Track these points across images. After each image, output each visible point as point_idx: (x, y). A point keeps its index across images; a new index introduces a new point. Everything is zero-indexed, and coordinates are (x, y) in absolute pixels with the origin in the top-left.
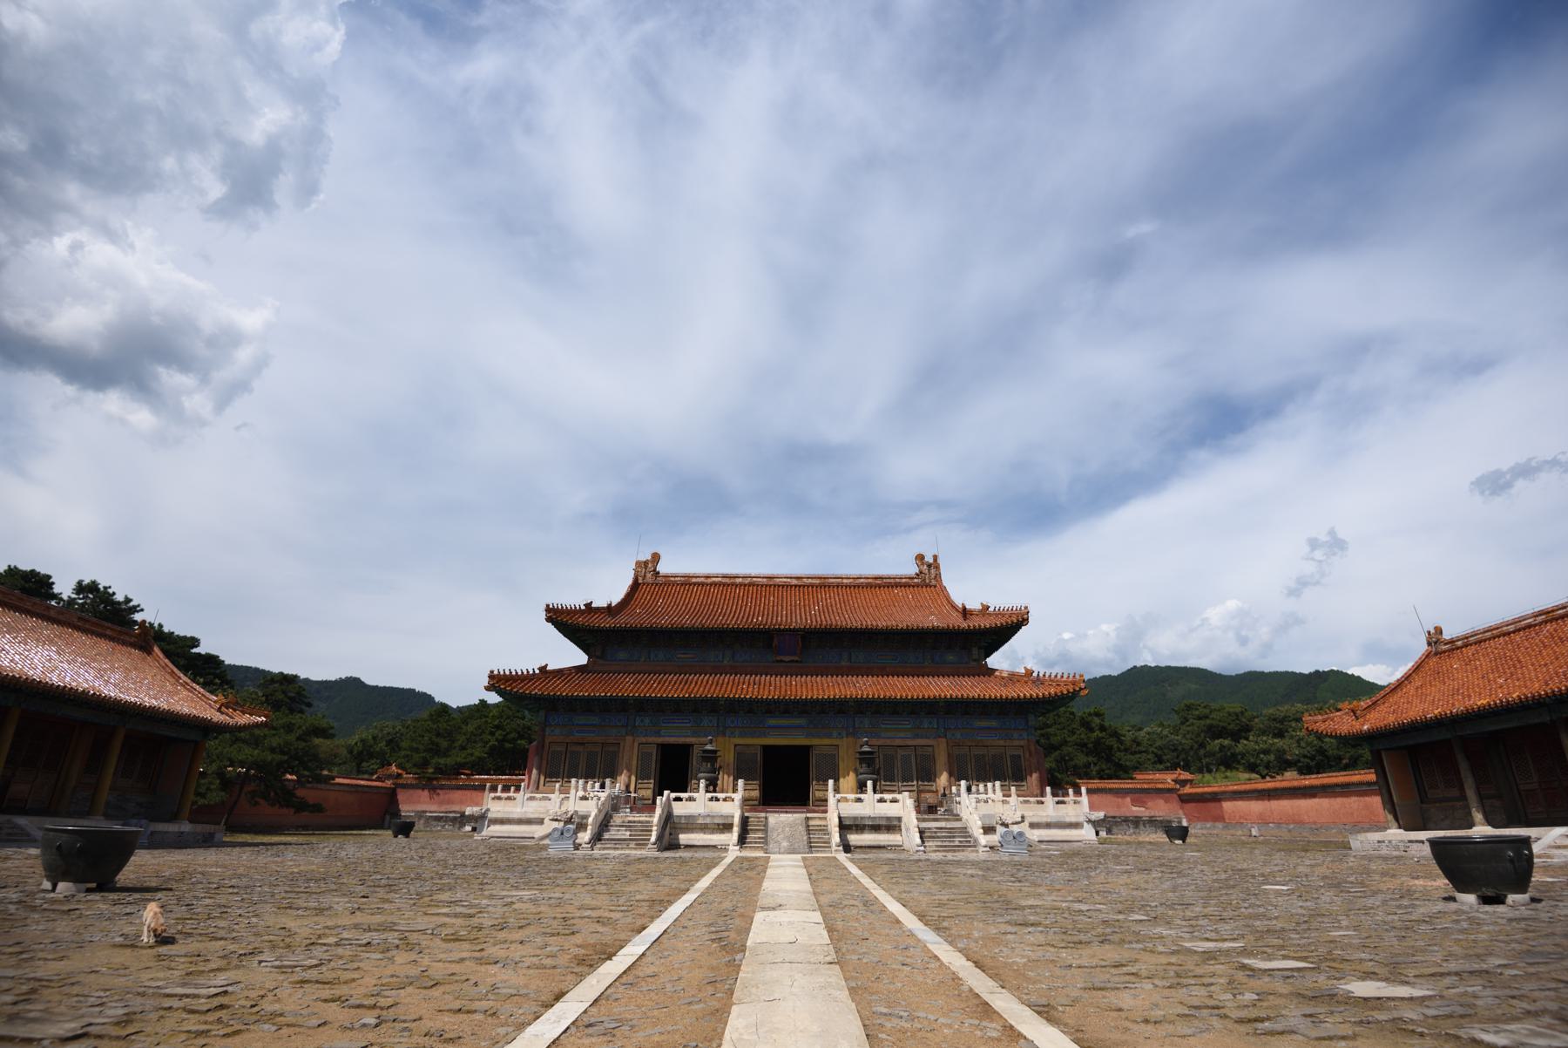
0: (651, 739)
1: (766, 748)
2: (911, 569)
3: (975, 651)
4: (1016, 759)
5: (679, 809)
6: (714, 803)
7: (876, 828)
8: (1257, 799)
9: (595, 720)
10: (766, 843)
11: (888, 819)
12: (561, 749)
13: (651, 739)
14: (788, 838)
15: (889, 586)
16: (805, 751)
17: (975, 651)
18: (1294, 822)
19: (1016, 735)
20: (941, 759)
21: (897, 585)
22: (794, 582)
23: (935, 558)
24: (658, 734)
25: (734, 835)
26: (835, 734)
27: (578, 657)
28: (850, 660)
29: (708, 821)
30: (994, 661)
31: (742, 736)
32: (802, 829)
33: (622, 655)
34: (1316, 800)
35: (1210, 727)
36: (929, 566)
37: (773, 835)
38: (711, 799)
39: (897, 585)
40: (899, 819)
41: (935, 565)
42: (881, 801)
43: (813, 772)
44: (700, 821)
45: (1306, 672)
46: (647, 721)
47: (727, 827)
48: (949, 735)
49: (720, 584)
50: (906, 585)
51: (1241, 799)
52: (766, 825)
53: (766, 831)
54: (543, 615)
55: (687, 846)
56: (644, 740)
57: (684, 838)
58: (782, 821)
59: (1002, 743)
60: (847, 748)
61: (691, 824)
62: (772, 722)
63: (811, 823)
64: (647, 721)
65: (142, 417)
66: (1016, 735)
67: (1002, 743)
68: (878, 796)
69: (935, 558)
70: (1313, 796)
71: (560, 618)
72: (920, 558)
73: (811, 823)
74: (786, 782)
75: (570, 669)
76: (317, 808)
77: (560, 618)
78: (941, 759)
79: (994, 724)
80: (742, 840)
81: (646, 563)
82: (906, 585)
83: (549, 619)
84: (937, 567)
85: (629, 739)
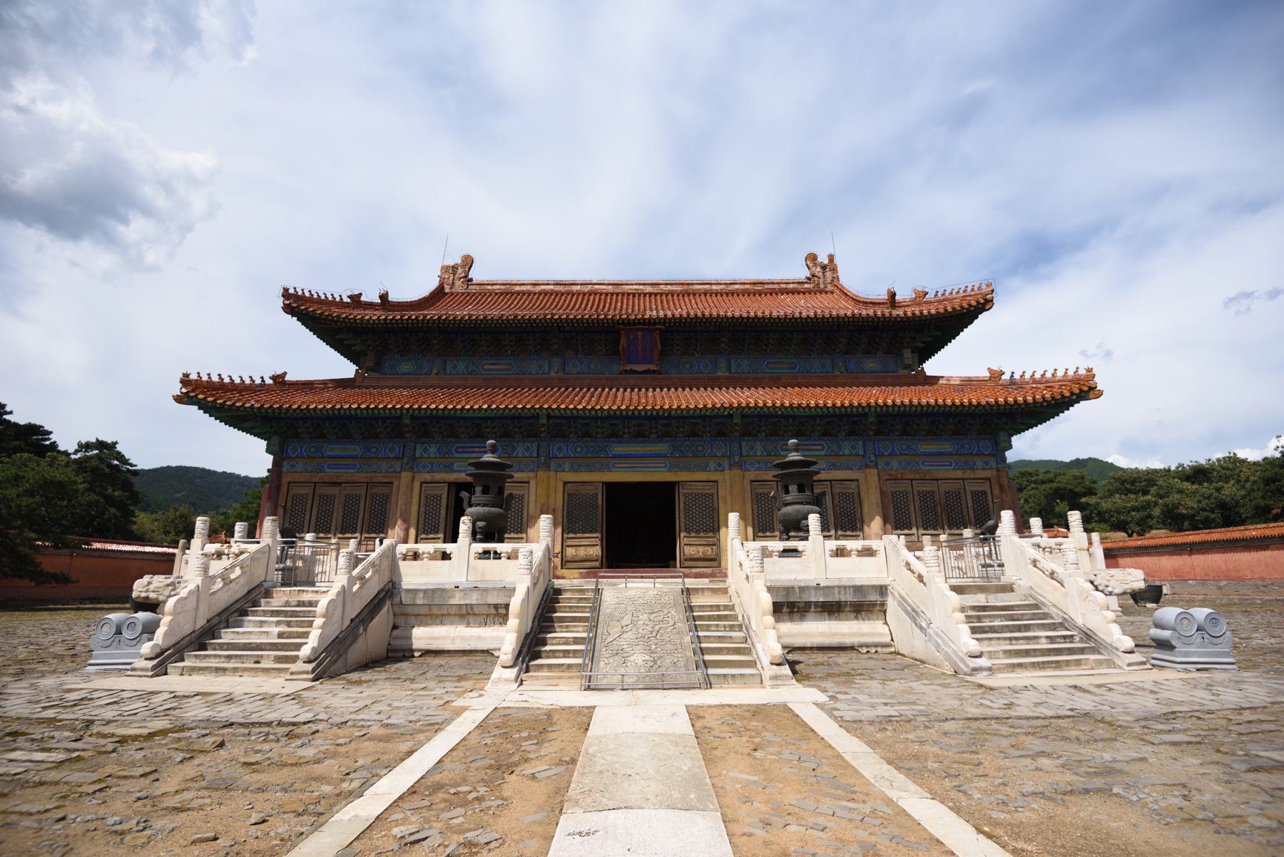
0: (439, 476)
1: (610, 487)
2: (801, 273)
3: (907, 354)
4: (979, 497)
5: (414, 576)
6: (491, 563)
7: (832, 609)
8: (1171, 554)
9: (355, 450)
10: (591, 654)
11: (858, 589)
12: (307, 491)
13: (439, 476)
14: (645, 641)
15: (771, 292)
16: (668, 489)
17: (907, 354)
18: (1228, 578)
19: (979, 463)
20: (871, 498)
21: (783, 292)
22: (649, 289)
23: (831, 258)
24: (449, 468)
25: (506, 638)
26: (712, 465)
27: (345, 369)
28: (729, 369)
29: (474, 599)
30: (931, 367)
31: (574, 470)
32: (676, 615)
33: (406, 367)
34: (1268, 553)
35: (1057, 490)
36: (824, 267)
37: (609, 632)
38: (485, 555)
39: (783, 292)
40: (882, 590)
41: (830, 266)
42: (840, 553)
43: (680, 519)
44: (456, 601)
45: (1067, 460)
46: (433, 450)
47: (499, 613)
48: (881, 464)
49: (551, 293)
50: (793, 292)
51: (1148, 554)
52: (596, 607)
53: (593, 623)
54: (280, 302)
55: (427, 653)
56: (428, 477)
57: (422, 636)
58: (633, 595)
59: (959, 474)
60: (729, 481)
61: (437, 608)
62: (619, 449)
63: (697, 601)
64: (433, 450)
65: (104, 260)
66: (979, 463)
67: (959, 474)
68: (833, 544)
69: (831, 258)
70: (1265, 548)
71: (302, 308)
72: (812, 258)
73: (697, 601)
74: (641, 533)
75: (325, 382)
76: (62, 579)
77: (302, 308)
78: (871, 498)
79: (948, 447)
80: (531, 649)
81: (454, 268)
82: (793, 292)
83: (288, 309)
84: (834, 270)
85: (406, 475)
